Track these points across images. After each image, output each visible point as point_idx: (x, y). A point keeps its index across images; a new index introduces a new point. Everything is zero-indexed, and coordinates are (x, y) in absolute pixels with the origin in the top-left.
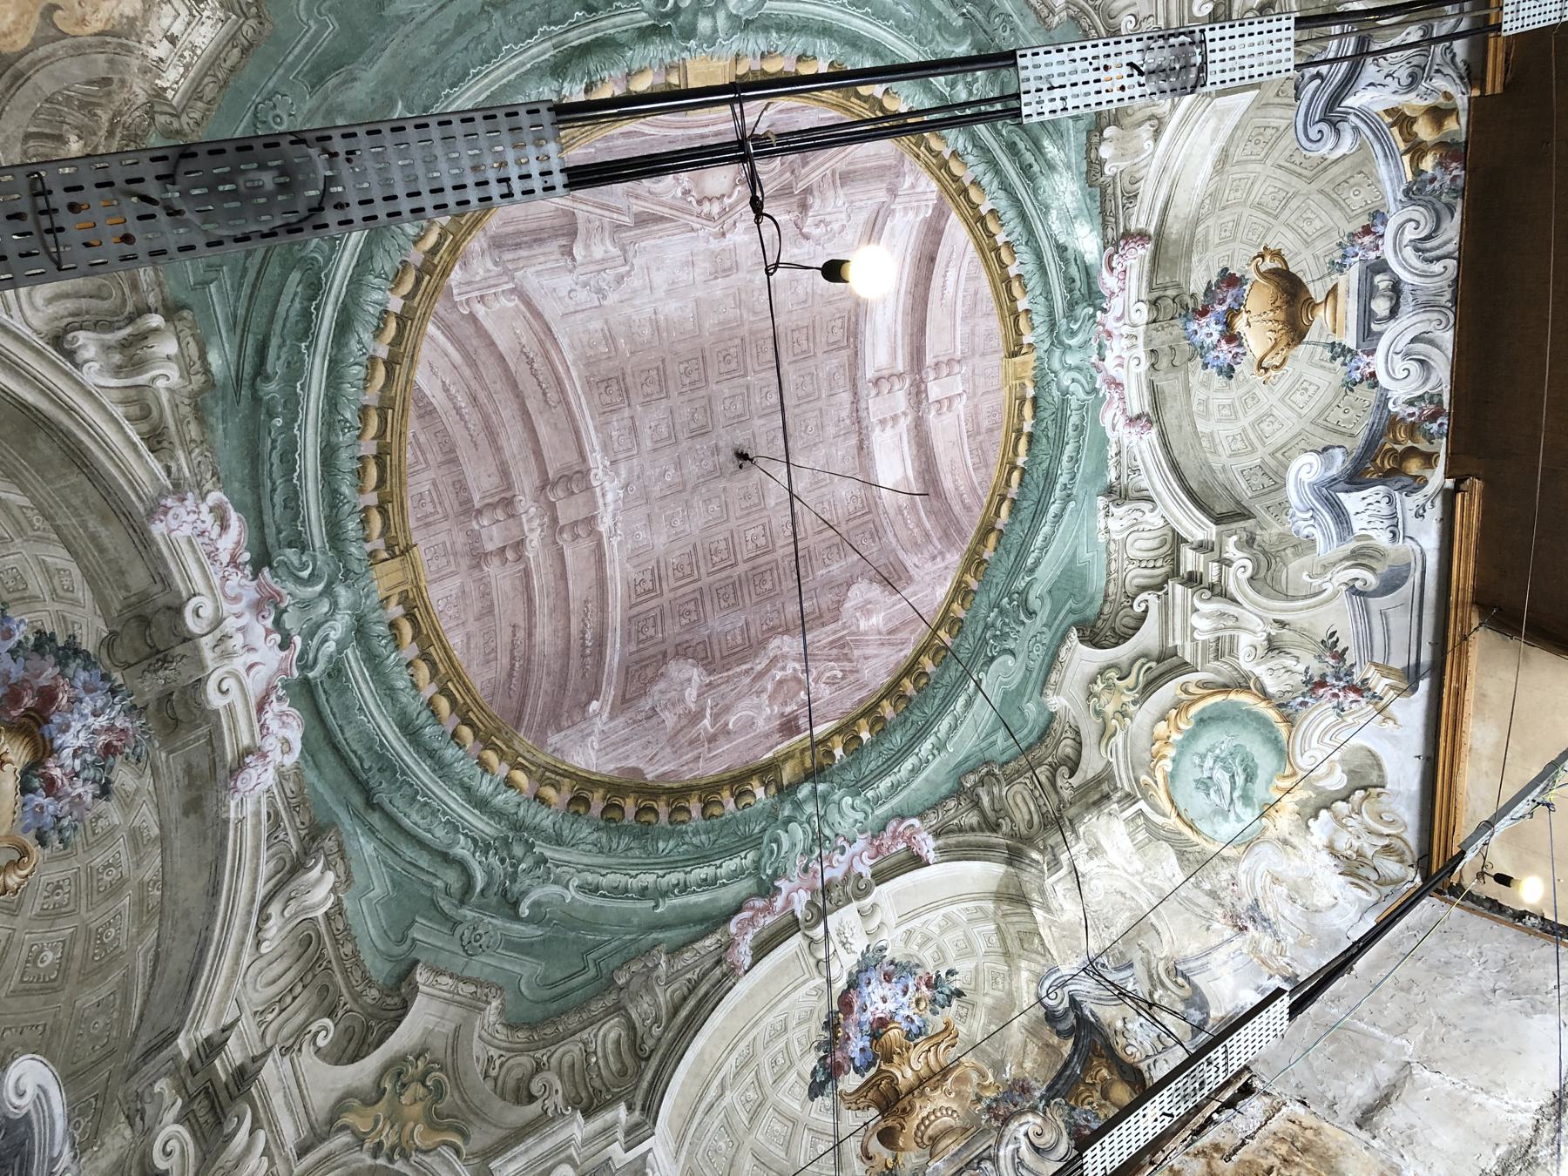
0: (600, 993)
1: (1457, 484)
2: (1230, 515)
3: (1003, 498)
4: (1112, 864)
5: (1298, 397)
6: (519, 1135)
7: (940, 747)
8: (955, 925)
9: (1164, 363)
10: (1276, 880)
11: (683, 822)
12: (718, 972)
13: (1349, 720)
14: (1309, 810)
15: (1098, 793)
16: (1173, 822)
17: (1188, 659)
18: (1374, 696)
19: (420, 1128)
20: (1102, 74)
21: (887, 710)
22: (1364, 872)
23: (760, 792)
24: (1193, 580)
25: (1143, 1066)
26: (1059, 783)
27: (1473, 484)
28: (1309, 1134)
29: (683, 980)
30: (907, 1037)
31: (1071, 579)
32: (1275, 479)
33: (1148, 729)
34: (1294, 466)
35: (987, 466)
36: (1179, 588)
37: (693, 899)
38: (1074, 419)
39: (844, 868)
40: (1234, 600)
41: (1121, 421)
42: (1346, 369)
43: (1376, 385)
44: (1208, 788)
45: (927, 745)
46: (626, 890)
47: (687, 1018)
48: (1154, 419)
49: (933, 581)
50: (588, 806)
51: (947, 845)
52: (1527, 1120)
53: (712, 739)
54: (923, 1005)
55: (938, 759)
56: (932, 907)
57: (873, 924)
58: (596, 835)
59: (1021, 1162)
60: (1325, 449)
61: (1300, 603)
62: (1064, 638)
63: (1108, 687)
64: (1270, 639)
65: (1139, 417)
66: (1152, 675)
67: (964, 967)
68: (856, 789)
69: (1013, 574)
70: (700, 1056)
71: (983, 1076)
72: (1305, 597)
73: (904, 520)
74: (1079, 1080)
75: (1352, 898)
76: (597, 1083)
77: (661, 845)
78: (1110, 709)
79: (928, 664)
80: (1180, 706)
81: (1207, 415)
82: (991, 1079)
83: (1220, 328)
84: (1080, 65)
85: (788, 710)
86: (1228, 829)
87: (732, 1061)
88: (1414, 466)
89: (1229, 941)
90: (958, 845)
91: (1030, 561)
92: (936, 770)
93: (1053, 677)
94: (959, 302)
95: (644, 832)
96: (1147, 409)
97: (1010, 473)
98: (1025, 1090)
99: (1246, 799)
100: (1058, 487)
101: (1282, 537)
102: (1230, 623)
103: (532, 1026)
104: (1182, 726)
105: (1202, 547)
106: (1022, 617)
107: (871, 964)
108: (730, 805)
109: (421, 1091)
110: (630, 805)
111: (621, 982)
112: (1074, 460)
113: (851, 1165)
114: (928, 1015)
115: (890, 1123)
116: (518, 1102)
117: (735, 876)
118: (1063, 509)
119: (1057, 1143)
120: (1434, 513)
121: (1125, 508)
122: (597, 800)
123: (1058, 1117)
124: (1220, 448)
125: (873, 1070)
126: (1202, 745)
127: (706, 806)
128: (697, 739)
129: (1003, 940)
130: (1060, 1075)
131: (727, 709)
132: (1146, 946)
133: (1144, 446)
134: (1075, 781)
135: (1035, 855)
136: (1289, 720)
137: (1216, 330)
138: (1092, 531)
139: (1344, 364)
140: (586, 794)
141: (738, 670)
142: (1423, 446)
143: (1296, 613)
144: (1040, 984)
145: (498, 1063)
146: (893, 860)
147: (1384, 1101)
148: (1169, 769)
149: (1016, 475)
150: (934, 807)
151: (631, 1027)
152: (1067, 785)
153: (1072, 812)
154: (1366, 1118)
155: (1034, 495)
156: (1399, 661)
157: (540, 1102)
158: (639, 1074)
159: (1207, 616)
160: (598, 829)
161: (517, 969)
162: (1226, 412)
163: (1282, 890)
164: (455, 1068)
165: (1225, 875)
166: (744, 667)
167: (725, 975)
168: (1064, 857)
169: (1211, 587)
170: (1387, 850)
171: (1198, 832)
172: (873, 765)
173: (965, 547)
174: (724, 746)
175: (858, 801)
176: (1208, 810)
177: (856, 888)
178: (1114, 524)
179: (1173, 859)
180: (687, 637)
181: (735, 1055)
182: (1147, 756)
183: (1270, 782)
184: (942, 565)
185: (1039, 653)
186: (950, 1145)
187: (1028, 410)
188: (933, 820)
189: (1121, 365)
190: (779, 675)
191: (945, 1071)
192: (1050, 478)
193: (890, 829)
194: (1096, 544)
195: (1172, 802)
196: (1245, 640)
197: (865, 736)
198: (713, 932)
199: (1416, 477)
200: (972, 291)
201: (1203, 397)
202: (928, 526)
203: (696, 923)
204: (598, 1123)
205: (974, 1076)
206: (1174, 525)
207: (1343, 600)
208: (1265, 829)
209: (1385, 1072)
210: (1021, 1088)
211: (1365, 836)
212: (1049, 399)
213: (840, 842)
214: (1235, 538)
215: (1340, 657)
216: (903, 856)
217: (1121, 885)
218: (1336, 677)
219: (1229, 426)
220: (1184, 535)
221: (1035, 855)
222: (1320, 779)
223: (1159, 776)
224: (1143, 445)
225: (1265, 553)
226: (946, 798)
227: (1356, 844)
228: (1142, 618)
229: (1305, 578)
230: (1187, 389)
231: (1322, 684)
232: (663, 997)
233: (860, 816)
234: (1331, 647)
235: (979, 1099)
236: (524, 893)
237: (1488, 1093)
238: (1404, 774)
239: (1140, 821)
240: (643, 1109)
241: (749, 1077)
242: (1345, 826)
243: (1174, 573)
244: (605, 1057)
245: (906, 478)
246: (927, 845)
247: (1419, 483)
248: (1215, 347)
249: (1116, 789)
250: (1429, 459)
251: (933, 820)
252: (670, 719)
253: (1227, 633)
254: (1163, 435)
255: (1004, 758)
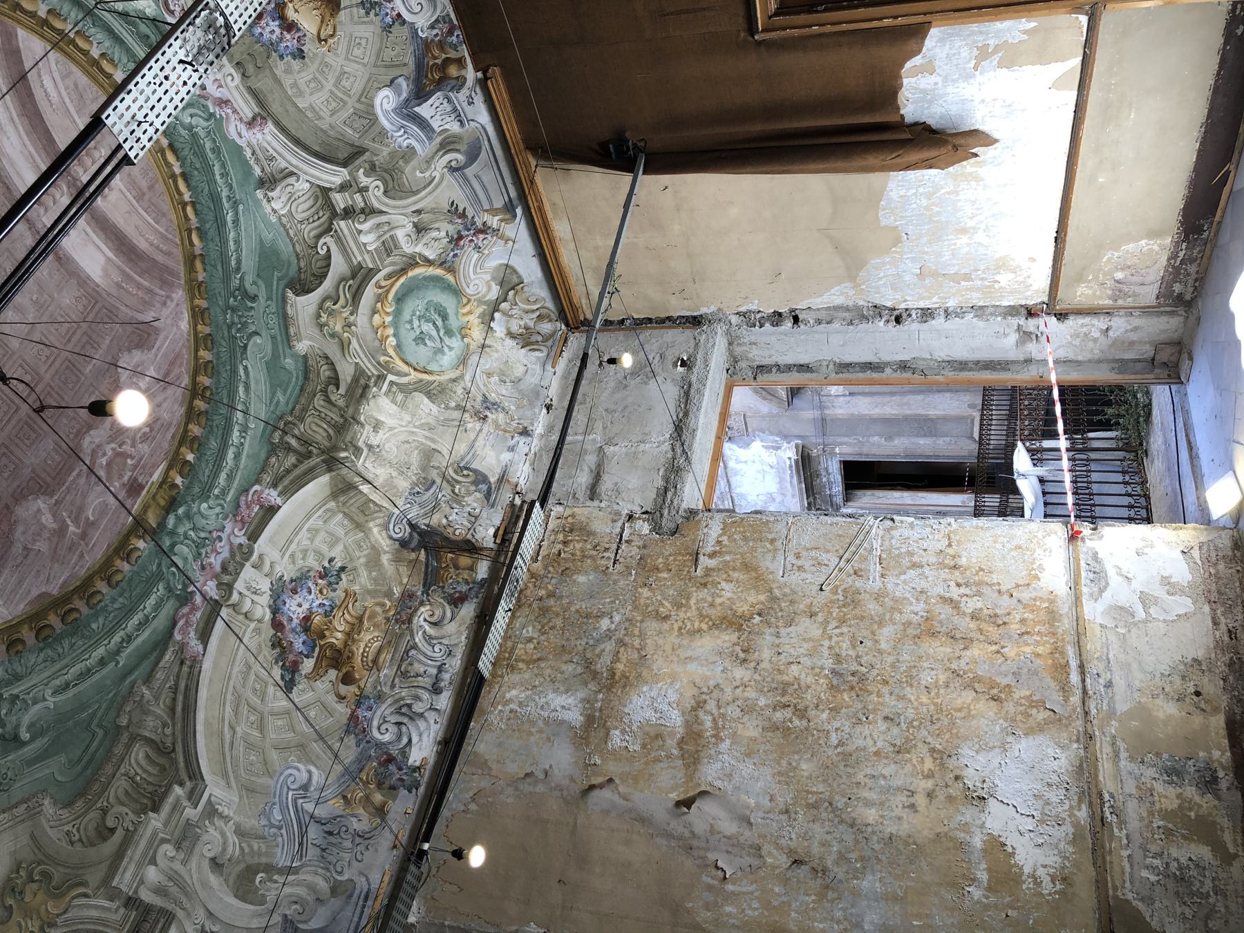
0: (115, 740)
1: (485, 73)
2: (349, 156)
3: (189, 231)
4: (392, 433)
5: (357, 52)
6: (119, 855)
7: (244, 429)
8: (317, 531)
9: (251, 69)
10: (489, 375)
11: (100, 601)
12: (185, 669)
13: (486, 252)
14: (487, 318)
15: (360, 389)
16: (414, 376)
17: (371, 266)
18: (494, 230)
19: (50, 904)
20: (167, 85)
21: (195, 430)
22: (533, 339)
23: (141, 544)
24: (349, 213)
25: (469, 537)
26: (333, 399)
27: (494, 72)
28: (570, 520)
29: (166, 691)
30: (326, 616)
31: (268, 257)
32: (367, 115)
33: (368, 325)
34: (377, 101)
35: (164, 215)
36: (342, 223)
37: (140, 640)
38: (208, 145)
39: (227, 548)
40: (382, 212)
41: (242, 128)
42: (380, 18)
43: (404, 22)
44: (423, 340)
45: (236, 434)
46: (89, 670)
47: (183, 709)
48: (264, 114)
49: (174, 321)
50: (22, 642)
51: (285, 487)
52: (666, 447)
53: (84, 536)
54: (325, 591)
55: (248, 438)
56: (296, 532)
57: (267, 567)
58: (42, 655)
59: (431, 637)
60: (392, 82)
61: (423, 193)
62: (284, 299)
63: (330, 314)
64: (415, 225)
65: (254, 119)
66: (354, 289)
67: (337, 552)
68: (205, 495)
69: (226, 279)
70: (207, 724)
71: (384, 605)
72: (425, 188)
73: (126, 290)
74: (438, 569)
75: (534, 360)
76: (150, 788)
77: (94, 626)
78: (338, 328)
79: (205, 380)
80: (381, 299)
81: (301, 94)
82: (389, 604)
83: (277, 23)
84: (148, 91)
85: (126, 478)
86: (448, 359)
87: (228, 709)
88: (453, 71)
89: (481, 430)
90: (292, 482)
91: (233, 263)
92: (250, 445)
93: (292, 331)
94: (67, 100)
95: (76, 627)
96: (257, 110)
97: (184, 210)
98: (411, 596)
99: (449, 333)
100: (224, 200)
101: (392, 155)
102: (386, 228)
103: (82, 794)
104: (388, 310)
105: (343, 188)
106: (250, 304)
107: (281, 590)
108: (126, 567)
109: (35, 886)
110: (53, 619)
111: (125, 723)
112: (225, 175)
113: (335, 710)
114: (332, 594)
115: (344, 671)
116: (105, 839)
117: (158, 606)
118: (237, 214)
119: (444, 613)
120: (479, 99)
121: (279, 188)
122: (27, 634)
123: (437, 598)
124: (322, 113)
125: (317, 649)
126: (406, 315)
127: (109, 580)
128: (73, 544)
129: (351, 519)
130: (426, 573)
131: (81, 509)
132: (437, 464)
133: (269, 138)
134: (342, 391)
135: (343, 455)
136: (452, 270)
137: (274, 25)
138: (265, 218)
139: (376, 15)
140: (15, 637)
141: (71, 478)
142: (453, 54)
143: (425, 200)
144: (387, 529)
145: (75, 831)
146: (256, 521)
147: (597, 477)
148: (394, 343)
149: (189, 209)
150: (263, 470)
151: (150, 742)
152: (337, 397)
153: (351, 411)
154: (593, 492)
155: (211, 216)
156: (498, 203)
157: (120, 827)
158: (174, 762)
159: (369, 232)
160: (41, 650)
161: (47, 771)
162: (312, 85)
163: (495, 379)
164: (48, 856)
165: (460, 391)
166: (74, 474)
167: (191, 667)
168: (361, 444)
169: (363, 211)
170: (540, 318)
171: (431, 373)
172: (207, 472)
173: (183, 282)
174: (95, 535)
175: (211, 502)
176: (430, 354)
177: (241, 555)
178: (276, 205)
179: (426, 400)
180: (16, 484)
181: (228, 704)
182: (377, 343)
183: (457, 314)
184: (173, 305)
185: (273, 321)
186: (386, 657)
187: (171, 157)
188: (267, 478)
189: (220, 86)
190: (104, 461)
191: (360, 619)
192: (215, 198)
193: (242, 503)
194: (272, 224)
195: (407, 363)
196: (400, 234)
197: (190, 457)
198: (166, 649)
199: (457, 78)
200: (72, 86)
201: (292, 81)
202: (146, 284)
203: (151, 653)
204: (166, 808)
205: (379, 609)
206: (318, 182)
207: (448, 177)
208: (468, 345)
209: (591, 459)
210: (408, 596)
211: (525, 316)
212: (182, 140)
213: (215, 534)
214: (362, 170)
215: (463, 215)
216: (261, 513)
217: (402, 438)
218: (466, 231)
219: (320, 94)
220: (328, 185)
221: (343, 455)
222: (485, 296)
223: (391, 351)
224: (267, 137)
225: (385, 171)
226: (267, 458)
227: (522, 323)
228: (328, 256)
229: (418, 174)
230: (278, 81)
231: (460, 238)
232: (160, 710)
233: (218, 510)
234: (455, 211)
235: (388, 620)
236: (17, 726)
237: (643, 442)
238: (530, 269)
239: (394, 388)
240: (190, 778)
241: (244, 710)
242: (511, 316)
243: (334, 215)
244: (145, 771)
245: (108, 259)
246: (272, 496)
247: (460, 82)
248: (281, 40)
249: (369, 378)
250: (460, 62)
251: (267, 478)
252: (42, 546)
253: (387, 236)
254: (277, 124)
255: (290, 406)
